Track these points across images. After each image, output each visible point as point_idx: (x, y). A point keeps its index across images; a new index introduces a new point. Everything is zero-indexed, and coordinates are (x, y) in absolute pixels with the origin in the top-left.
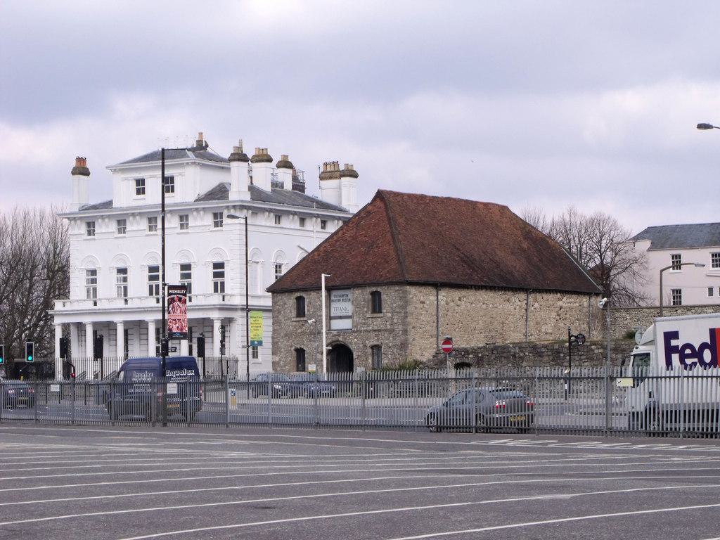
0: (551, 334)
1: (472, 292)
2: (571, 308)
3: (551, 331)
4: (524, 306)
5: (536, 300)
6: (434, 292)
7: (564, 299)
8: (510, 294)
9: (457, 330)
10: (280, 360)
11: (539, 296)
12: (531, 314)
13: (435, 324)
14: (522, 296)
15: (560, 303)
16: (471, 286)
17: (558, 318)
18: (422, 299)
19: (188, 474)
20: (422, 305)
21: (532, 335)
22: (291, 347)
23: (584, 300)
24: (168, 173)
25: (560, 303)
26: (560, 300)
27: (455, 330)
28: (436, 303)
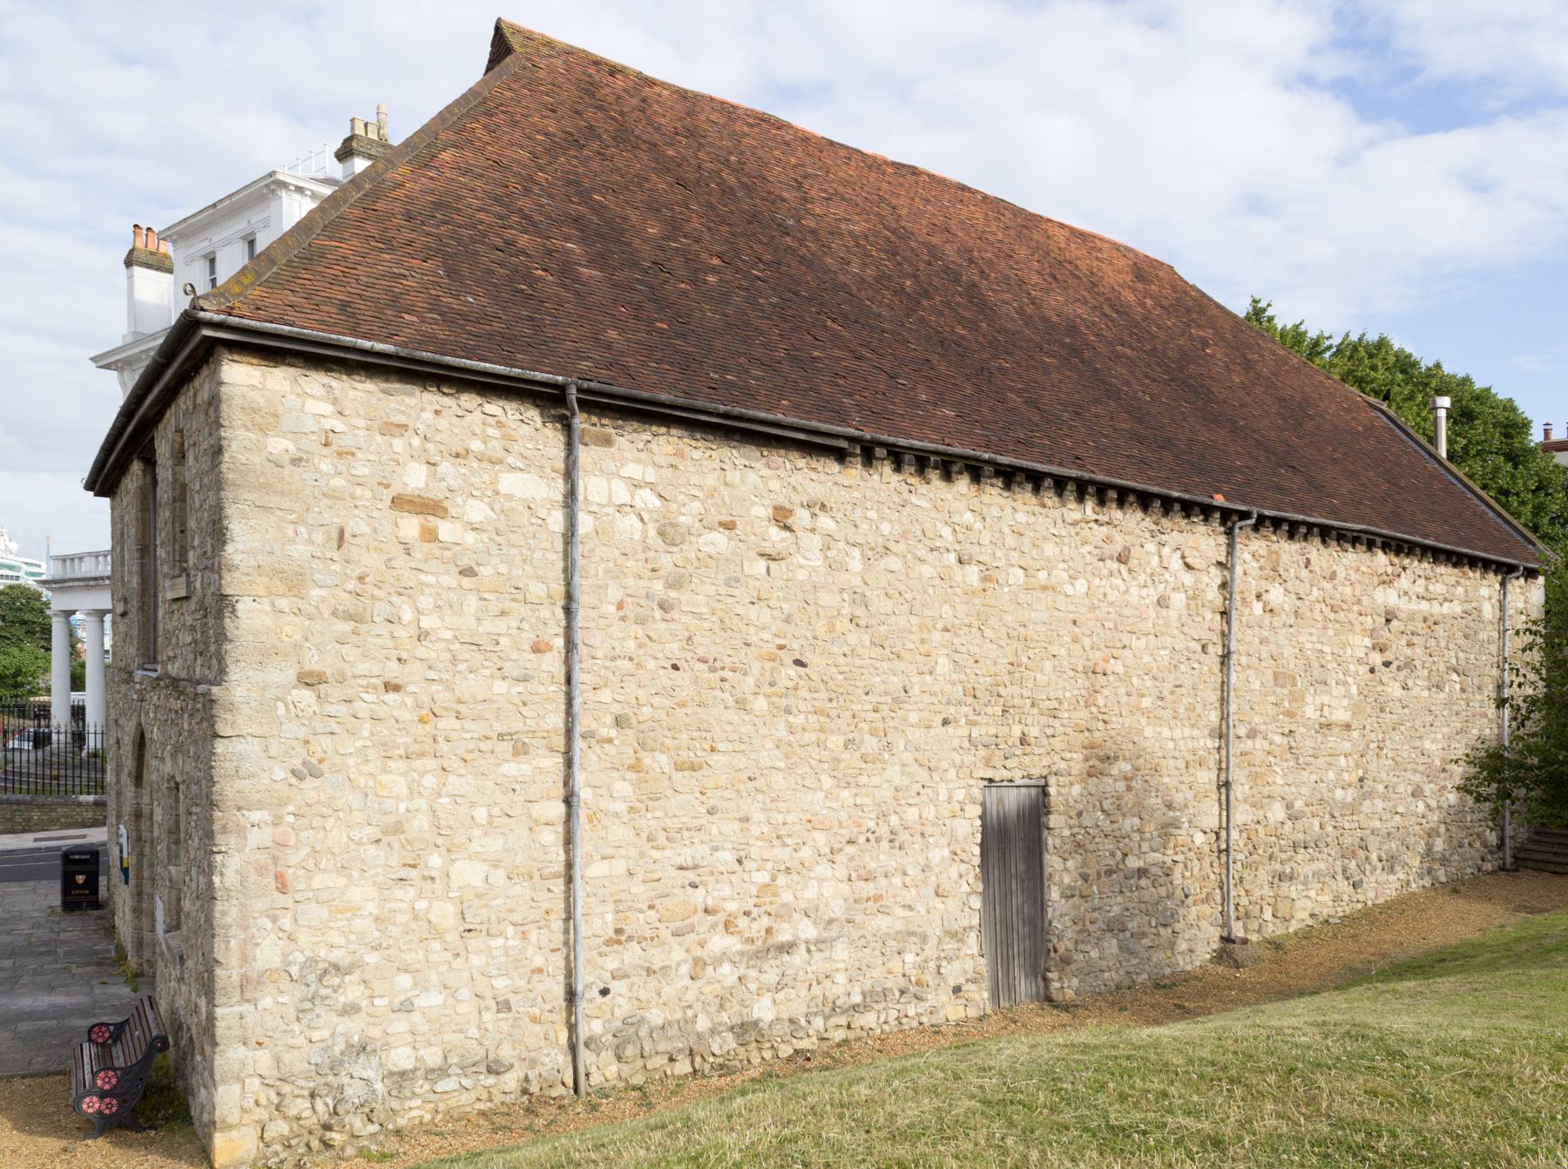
0: (1348, 726)
1: (884, 481)
2: (1431, 622)
3: (1342, 716)
4: (1213, 595)
5: (1275, 572)
6: (551, 439)
7: (1404, 582)
8: (1132, 521)
9: (761, 704)
11: (1289, 551)
12: (1252, 637)
13: (553, 663)
14: (1204, 540)
15: (1388, 597)
16: (1310, 526)
17: (1377, 659)
18: (415, 479)
19: (719, 415)
20: (410, 526)
21: (1252, 734)
23: (1485, 591)
24: (1460, 763)
25: (1388, 597)
26: (1386, 582)
27: (742, 705)
28: (557, 520)
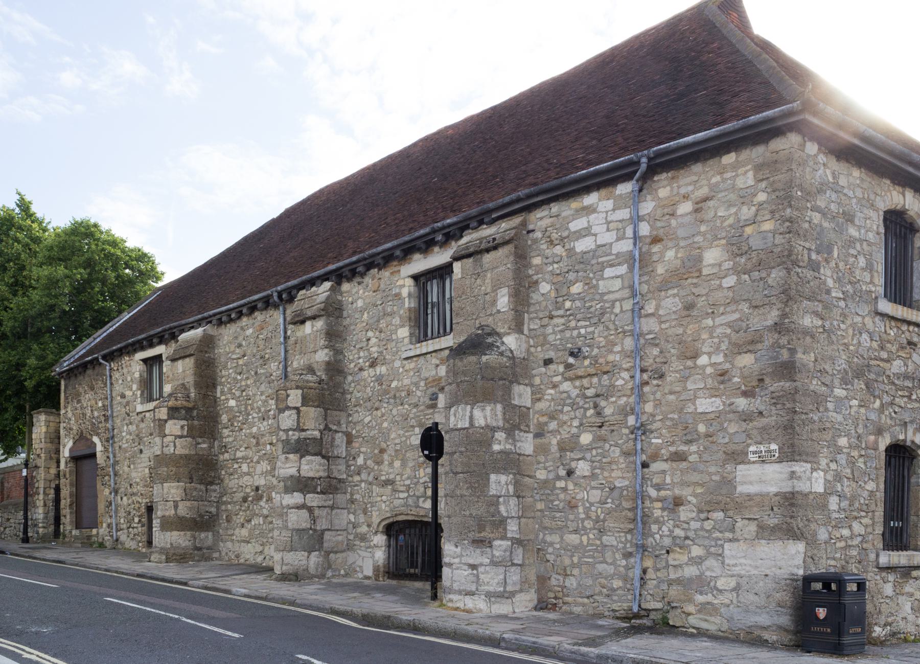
10: (827, 493)
22: (879, 432)
